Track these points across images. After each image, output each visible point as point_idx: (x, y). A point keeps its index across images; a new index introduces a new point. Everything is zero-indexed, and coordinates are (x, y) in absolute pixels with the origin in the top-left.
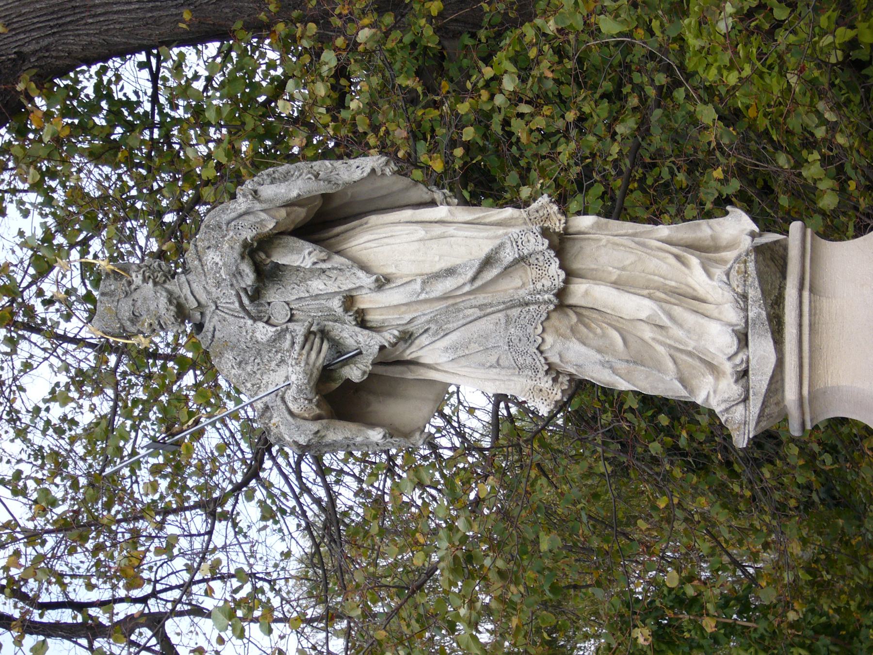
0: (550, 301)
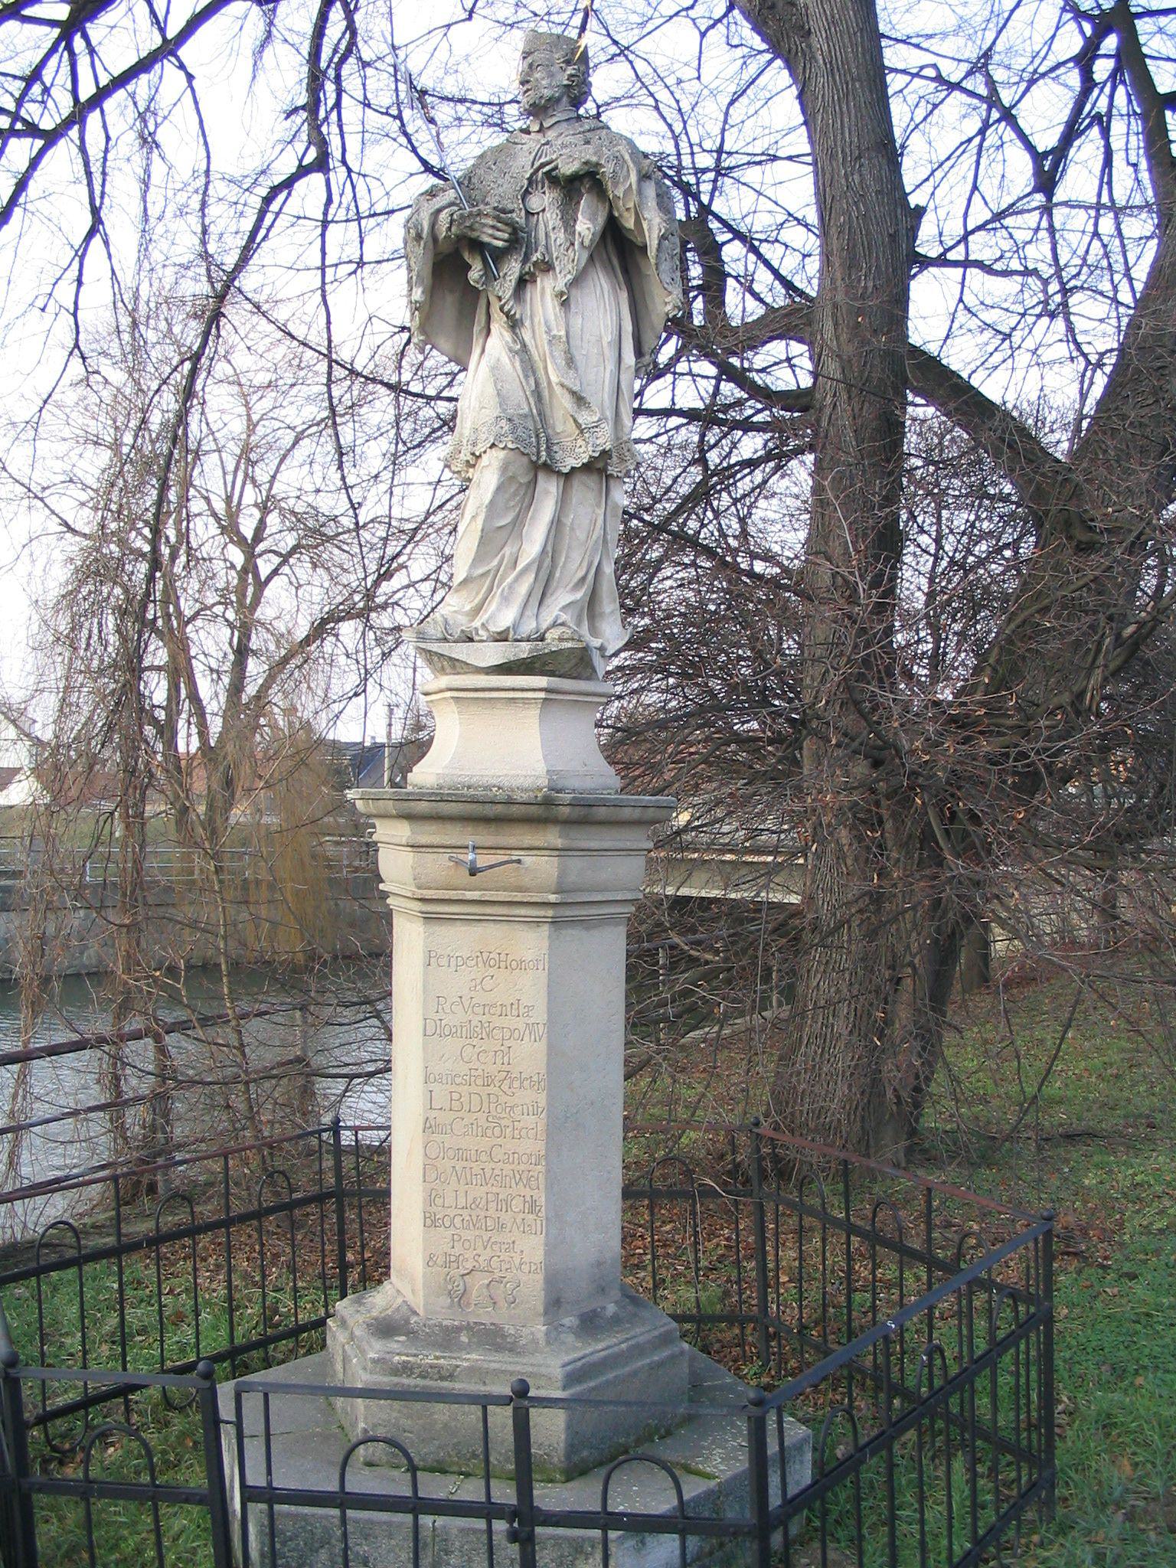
0: (539, 457)
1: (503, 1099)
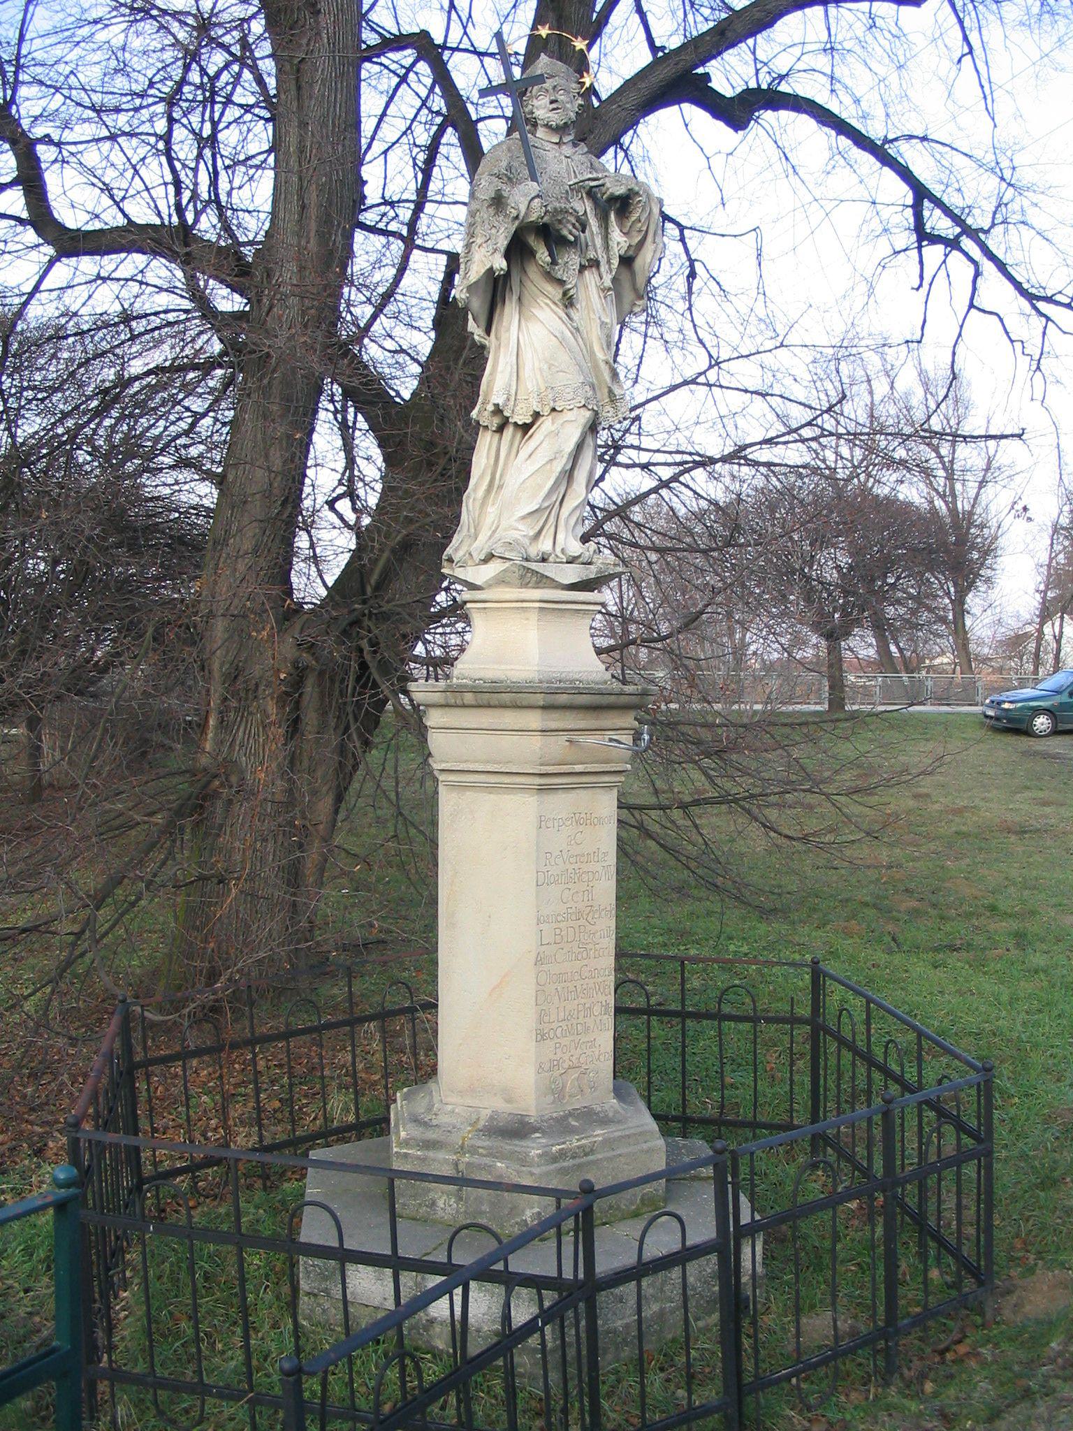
1: (589, 927)
